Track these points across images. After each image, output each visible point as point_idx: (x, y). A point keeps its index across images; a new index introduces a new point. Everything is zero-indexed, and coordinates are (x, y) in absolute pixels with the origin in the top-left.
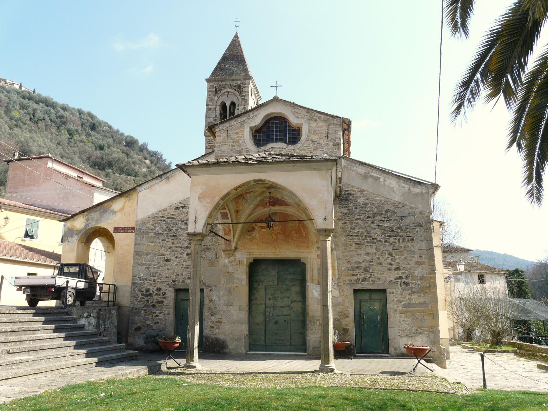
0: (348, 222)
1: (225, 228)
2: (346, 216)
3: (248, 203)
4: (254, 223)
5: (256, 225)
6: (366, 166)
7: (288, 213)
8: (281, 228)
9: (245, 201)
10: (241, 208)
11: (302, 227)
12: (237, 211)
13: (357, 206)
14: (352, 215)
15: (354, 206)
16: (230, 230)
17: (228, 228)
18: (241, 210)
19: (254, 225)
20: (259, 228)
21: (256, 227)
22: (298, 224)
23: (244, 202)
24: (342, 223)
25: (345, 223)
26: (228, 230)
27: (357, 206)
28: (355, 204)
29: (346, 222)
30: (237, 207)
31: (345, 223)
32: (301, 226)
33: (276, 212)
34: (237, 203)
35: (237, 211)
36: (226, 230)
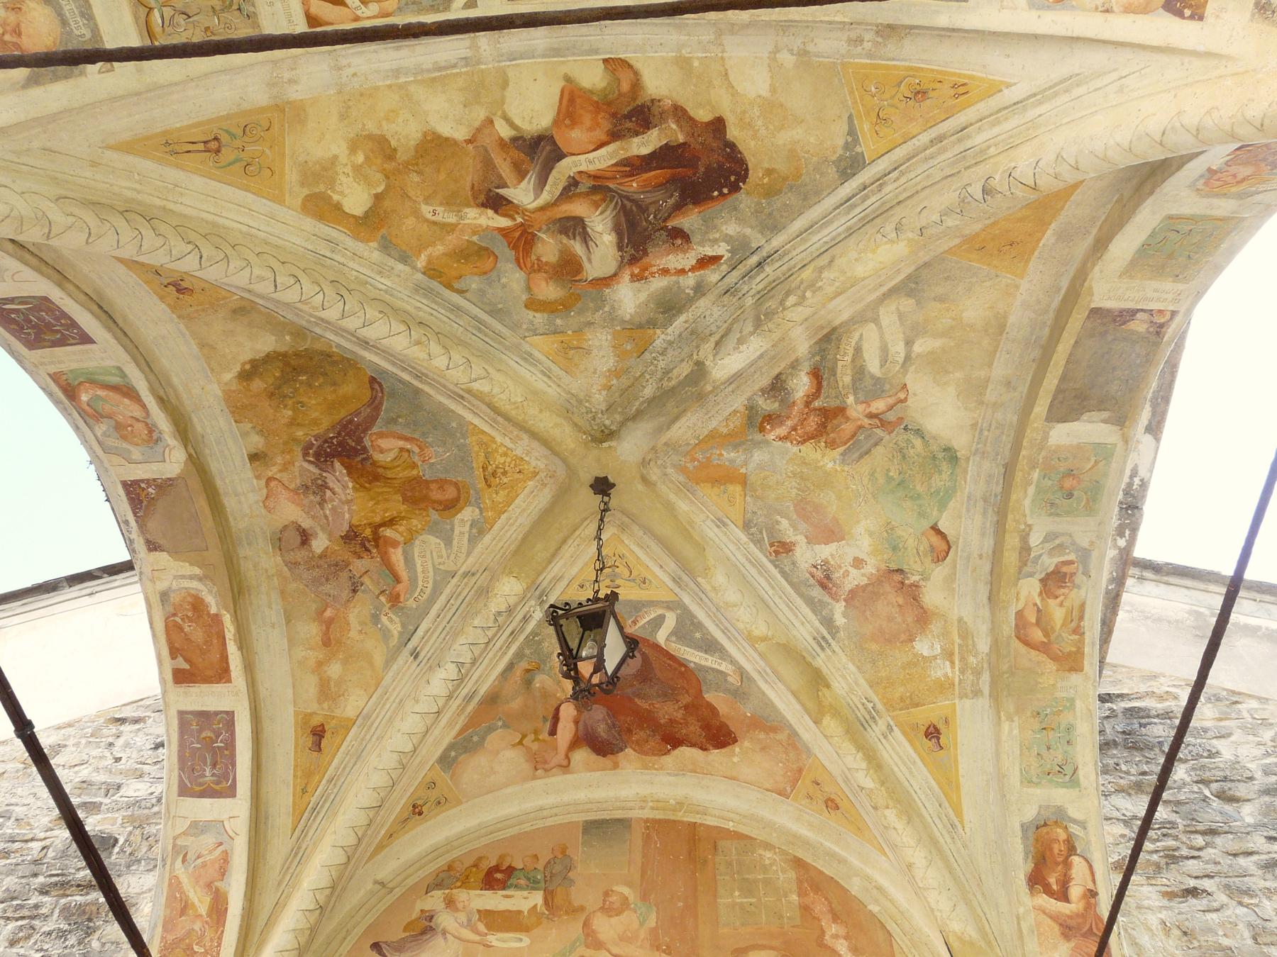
0: (1206, 884)
1: (185, 880)
2: (1171, 843)
3: (415, 654)
4: (439, 885)
5: (450, 903)
6: (1189, 582)
7: (711, 821)
8: (652, 921)
9: (396, 629)
10: (352, 705)
11: (836, 918)
12: (318, 734)
13: (1225, 779)
14: (1219, 840)
15: (1206, 782)
16: (218, 910)
17: (209, 885)
18: (347, 725)
19: (434, 901)
20: (470, 926)
21: (446, 920)
22: (794, 897)
23: (386, 634)
24: (1170, 895)
25: (1193, 892)
26: (201, 902)
27: (1225, 779)
28: (1203, 767)
29: (1192, 883)
30: (327, 691)
31: (1193, 892)
32: (820, 908)
33: (618, 814)
34: (326, 642)
35: (318, 734)
36: (185, 907)
